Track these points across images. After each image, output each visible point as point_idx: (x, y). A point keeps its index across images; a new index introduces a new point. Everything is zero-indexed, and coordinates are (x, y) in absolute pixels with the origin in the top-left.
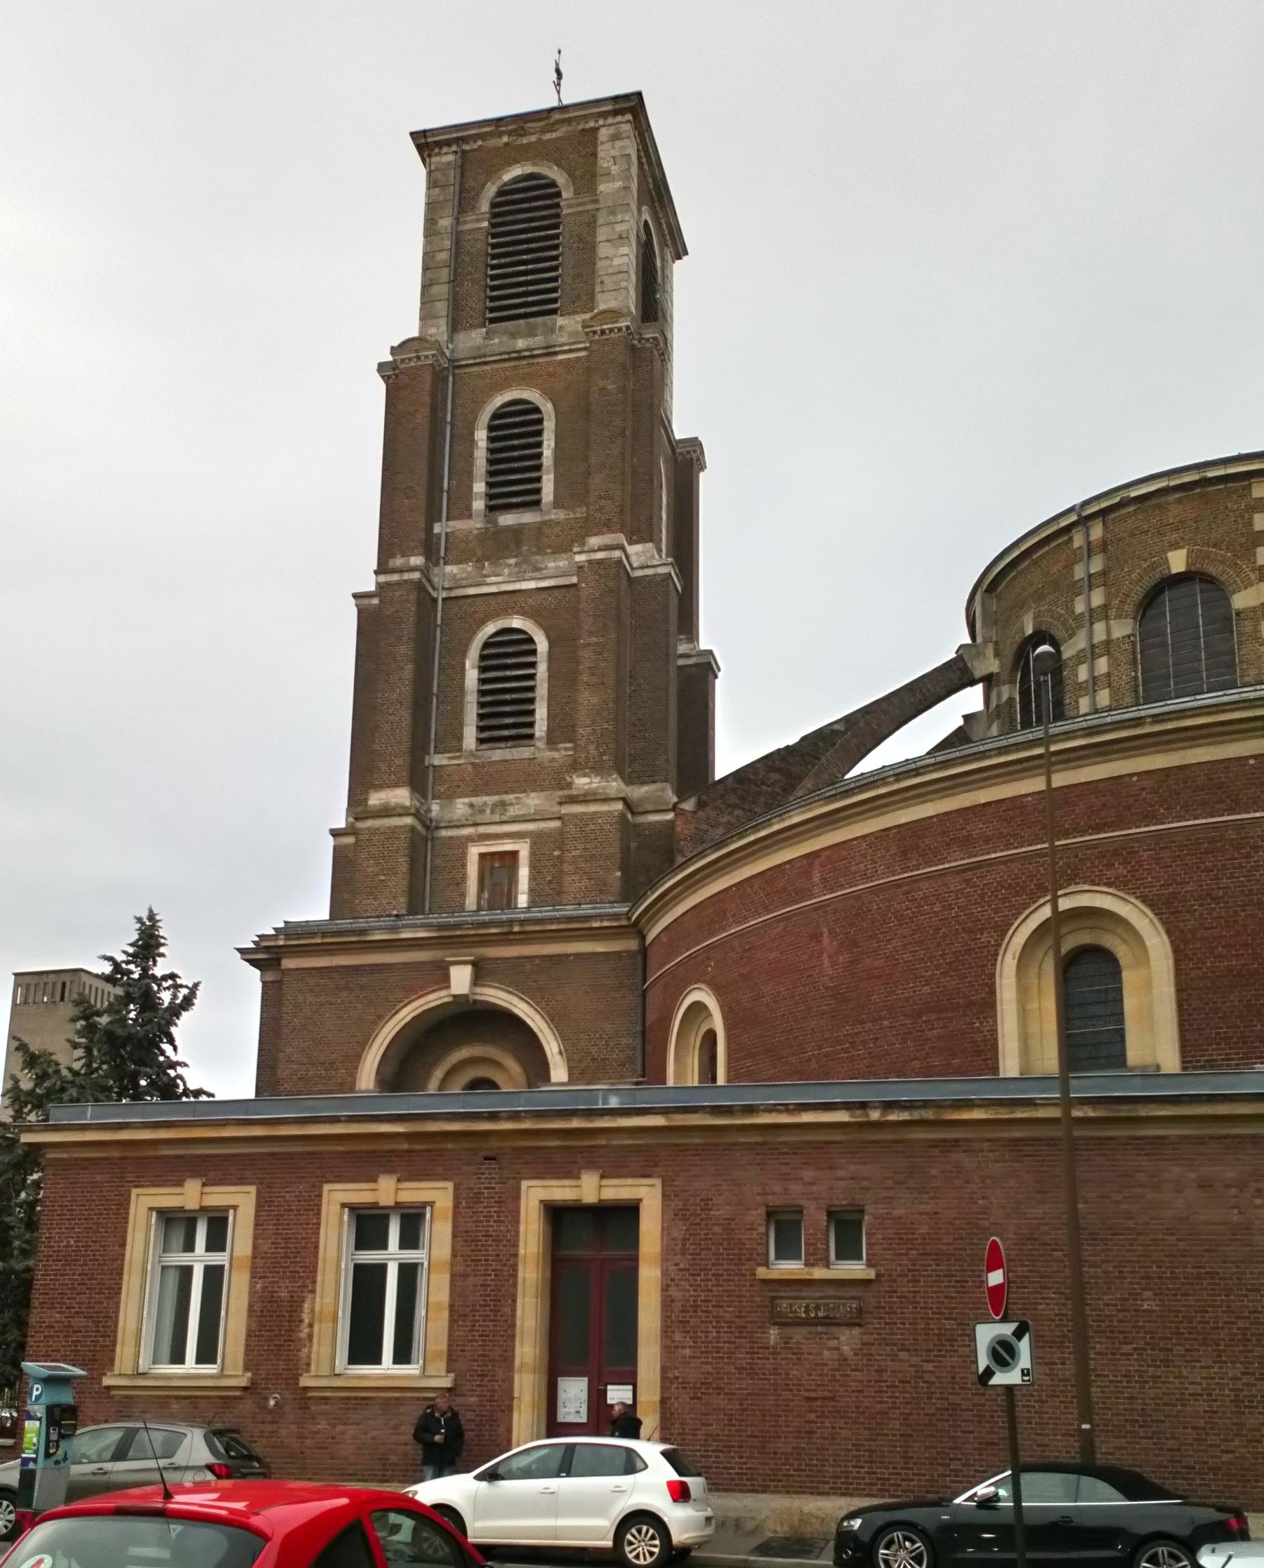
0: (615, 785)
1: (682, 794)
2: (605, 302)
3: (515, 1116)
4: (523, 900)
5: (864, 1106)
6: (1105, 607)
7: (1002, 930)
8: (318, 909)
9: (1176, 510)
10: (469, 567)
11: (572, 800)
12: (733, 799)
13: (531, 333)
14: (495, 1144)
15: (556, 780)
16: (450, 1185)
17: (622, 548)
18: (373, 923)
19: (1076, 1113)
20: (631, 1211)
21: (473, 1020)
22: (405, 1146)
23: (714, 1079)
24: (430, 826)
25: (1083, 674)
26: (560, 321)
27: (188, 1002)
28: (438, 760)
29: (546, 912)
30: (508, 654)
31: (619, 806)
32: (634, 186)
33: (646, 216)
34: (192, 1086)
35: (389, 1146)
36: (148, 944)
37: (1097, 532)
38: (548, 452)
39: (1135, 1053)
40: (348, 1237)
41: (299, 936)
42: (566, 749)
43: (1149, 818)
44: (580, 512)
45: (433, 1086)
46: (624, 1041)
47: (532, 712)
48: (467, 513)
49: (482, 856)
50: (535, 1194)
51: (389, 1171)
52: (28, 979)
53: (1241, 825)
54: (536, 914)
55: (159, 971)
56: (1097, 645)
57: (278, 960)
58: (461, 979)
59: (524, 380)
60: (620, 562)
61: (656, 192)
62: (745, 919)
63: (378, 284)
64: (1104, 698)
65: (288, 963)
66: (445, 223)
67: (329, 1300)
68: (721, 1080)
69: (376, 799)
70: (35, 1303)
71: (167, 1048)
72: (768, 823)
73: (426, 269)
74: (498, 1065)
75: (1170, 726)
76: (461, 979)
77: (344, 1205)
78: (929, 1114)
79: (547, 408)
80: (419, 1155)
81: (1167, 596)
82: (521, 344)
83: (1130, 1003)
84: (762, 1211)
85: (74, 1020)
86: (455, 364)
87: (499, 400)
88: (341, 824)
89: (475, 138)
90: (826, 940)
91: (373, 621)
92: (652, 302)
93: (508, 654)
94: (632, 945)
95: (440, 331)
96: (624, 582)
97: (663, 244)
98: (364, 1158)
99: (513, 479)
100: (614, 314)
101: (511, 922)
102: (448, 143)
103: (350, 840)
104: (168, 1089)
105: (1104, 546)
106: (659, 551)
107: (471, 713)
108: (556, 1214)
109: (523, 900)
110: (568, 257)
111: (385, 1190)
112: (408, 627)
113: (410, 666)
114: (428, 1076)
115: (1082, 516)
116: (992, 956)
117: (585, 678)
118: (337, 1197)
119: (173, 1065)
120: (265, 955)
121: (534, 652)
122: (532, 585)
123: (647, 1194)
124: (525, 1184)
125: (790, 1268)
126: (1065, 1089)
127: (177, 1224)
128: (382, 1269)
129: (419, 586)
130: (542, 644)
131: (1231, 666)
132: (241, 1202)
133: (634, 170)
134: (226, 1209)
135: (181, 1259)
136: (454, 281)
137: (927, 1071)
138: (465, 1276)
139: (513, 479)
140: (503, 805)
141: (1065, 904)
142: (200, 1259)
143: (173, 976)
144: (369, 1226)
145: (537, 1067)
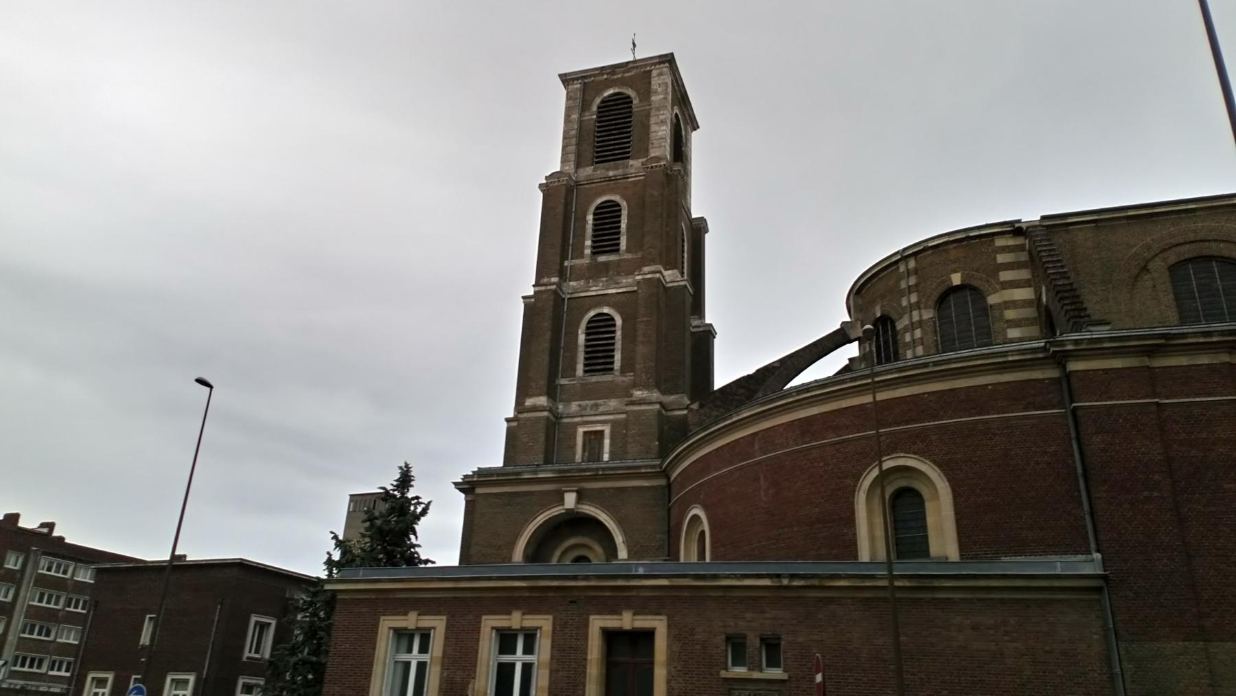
0: (655, 395)
1: (693, 400)
2: (654, 153)
3: (586, 578)
4: (606, 457)
5: (778, 576)
6: (918, 302)
7: (857, 477)
8: (497, 461)
9: (953, 253)
10: (582, 282)
11: (633, 403)
12: (719, 403)
13: (617, 169)
14: (576, 593)
15: (623, 392)
16: (550, 617)
17: (660, 272)
18: (525, 469)
19: (897, 584)
20: (649, 635)
21: (577, 523)
22: (527, 594)
23: (704, 559)
24: (558, 417)
25: (908, 338)
26: (631, 162)
27: (424, 512)
28: (563, 381)
29: (617, 464)
30: (601, 326)
31: (658, 406)
32: (670, 98)
33: (676, 110)
34: (423, 557)
35: (516, 594)
36: (405, 480)
37: (912, 264)
38: (623, 225)
39: (934, 550)
40: (495, 647)
41: (485, 476)
42: (1094, 350)
43: (935, 418)
44: (639, 255)
45: (554, 561)
46: (658, 536)
47: (613, 357)
48: (582, 256)
49: (585, 433)
50: (597, 623)
51: (518, 608)
52: (359, 499)
53: (987, 421)
54: (611, 465)
55: (410, 495)
56: (915, 320)
57: (473, 489)
58: (570, 500)
59: (612, 191)
60: (659, 279)
61: (681, 98)
62: (720, 469)
63: (541, 147)
64: (920, 350)
65: (479, 491)
66: (575, 116)
67: (483, 682)
68: (708, 560)
69: (529, 402)
70: (326, 681)
71: (412, 537)
72: (730, 417)
73: (564, 138)
74: (590, 548)
75: (943, 367)
76: (570, 500)
77: (493, 628)
78: (816, 582)
79: (624, 204)
80: (533, 600)
81: (951, 297)
82: (611, 173)
83: (930, 520)
84: (723, 637)
85: (364, 521)
86: (577, 184)
87: (599, 201)
88: (511, 415)
89: (594, 76)
90: (762, 480)
91: (532, 309)
92: (680, 151)
93: (601, 326)
94: (662, 482)
95: (570, 168)
96: (661, 289)
97: (686, 124)
98: (506, 601)
99: (606, 238)
100: (658, 159)
101: (597, 469)
102: (577, 79)
103: (515, 424)
104: (412, 560)
105: (916, 271)
106: (682, 273)
107: (581, 356)
108: (610, 636)
109: (606, 457)
110: (635, 131)
111: (515, 620)
112: (549, 313)
113: (549, 333)
114: (552, 555)
115: (904, 256)
116: (852, 492)
117: (640, 338)
118: (490, 622)
119: (414, 546)
120: (467, 486)
121: (614, 325)
122: (614, 291)
123: (659, 625)
124: (592, 617)
125: (740, 671)
126: (890, 570)
127: (403, 637)
128: (513, 665)
129: (555, 292)
130: (619, 321)
131: (989, 334)
132: (438, 624)
133: (670, 89)
134: (430, 629)
135: (404, 657)
136: (578, 144)
137: (819, 557)
138: (557, 671)
139: (606, 238)
140: (597, 406)
141: (886, 466)
142: (415, 658)
143: (417, 498)
144: (506, 641)
145: (612, 551)
